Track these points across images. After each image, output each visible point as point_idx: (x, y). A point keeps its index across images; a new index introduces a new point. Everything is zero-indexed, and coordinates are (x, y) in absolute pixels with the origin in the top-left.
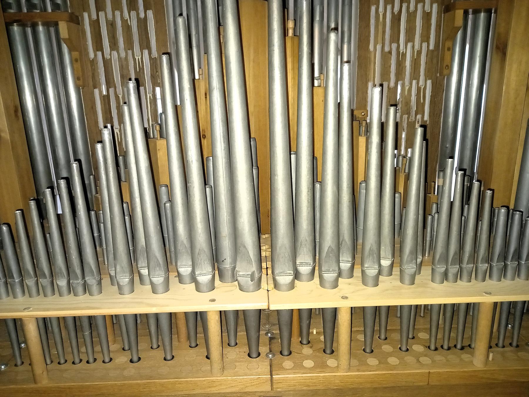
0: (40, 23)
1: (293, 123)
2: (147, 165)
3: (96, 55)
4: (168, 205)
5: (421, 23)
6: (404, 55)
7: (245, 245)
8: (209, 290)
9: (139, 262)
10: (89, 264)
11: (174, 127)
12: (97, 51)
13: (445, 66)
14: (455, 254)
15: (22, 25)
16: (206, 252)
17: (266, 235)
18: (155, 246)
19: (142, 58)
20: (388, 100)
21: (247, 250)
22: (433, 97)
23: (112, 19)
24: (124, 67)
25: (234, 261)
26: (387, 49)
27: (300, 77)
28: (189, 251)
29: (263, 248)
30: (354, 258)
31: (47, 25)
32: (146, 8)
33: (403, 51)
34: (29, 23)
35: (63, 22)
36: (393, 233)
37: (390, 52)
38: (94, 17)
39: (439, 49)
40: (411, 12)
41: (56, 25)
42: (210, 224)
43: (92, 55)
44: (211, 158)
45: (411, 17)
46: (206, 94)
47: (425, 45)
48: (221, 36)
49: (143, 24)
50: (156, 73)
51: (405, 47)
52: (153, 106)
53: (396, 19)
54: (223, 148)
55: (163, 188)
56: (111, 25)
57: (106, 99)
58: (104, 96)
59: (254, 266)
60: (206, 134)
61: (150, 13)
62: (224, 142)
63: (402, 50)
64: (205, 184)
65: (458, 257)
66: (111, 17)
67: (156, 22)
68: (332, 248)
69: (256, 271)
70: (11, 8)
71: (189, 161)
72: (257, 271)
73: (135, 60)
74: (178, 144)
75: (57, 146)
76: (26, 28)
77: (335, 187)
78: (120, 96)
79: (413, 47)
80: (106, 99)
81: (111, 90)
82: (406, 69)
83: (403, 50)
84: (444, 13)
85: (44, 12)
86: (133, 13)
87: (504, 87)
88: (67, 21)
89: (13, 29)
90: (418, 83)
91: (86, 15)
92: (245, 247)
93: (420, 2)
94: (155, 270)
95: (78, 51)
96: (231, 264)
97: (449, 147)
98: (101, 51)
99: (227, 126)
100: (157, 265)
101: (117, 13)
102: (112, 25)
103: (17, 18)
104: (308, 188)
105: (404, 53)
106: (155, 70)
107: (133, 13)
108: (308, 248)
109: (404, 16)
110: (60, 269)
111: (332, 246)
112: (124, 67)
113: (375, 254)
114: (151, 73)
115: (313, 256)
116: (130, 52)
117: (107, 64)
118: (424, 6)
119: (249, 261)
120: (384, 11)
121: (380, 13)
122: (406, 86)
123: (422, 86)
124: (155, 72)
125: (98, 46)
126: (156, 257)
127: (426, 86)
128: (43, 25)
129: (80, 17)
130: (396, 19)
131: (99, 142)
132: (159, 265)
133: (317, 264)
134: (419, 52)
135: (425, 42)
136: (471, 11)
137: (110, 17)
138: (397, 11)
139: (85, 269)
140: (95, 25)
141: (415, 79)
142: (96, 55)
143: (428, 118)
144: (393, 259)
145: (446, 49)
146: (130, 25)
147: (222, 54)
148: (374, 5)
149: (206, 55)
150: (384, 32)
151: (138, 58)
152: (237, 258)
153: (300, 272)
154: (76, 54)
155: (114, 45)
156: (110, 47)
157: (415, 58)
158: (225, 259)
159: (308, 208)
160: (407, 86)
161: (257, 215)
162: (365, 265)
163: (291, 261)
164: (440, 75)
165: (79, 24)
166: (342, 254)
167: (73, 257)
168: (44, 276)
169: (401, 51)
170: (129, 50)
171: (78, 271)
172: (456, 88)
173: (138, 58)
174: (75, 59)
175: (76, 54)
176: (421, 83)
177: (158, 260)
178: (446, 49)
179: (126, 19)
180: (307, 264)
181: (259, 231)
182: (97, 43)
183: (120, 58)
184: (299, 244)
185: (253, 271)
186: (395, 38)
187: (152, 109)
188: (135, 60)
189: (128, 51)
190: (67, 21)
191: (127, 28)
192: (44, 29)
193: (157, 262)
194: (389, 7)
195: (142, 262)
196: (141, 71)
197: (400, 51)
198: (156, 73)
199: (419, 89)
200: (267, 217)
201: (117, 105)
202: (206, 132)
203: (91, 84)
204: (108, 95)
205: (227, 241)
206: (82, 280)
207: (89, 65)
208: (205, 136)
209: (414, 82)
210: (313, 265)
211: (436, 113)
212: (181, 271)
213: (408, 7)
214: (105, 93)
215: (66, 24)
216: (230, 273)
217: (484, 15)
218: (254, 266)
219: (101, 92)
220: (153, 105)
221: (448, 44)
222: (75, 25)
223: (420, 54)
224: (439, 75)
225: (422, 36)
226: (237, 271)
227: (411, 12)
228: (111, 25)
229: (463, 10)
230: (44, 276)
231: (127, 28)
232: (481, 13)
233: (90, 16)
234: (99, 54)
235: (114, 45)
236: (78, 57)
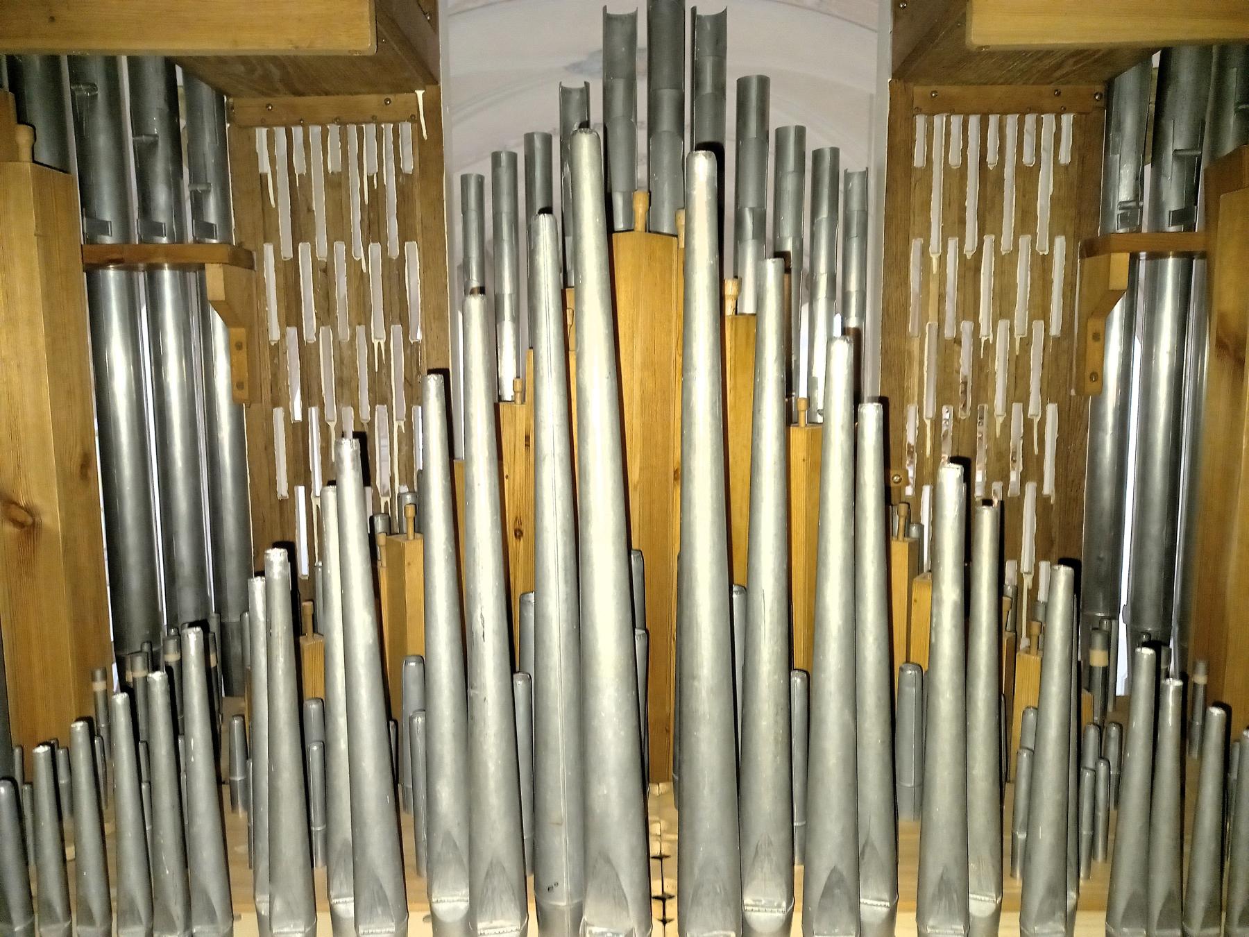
0: (166, 265)
1: (739, 522)
2: (371, 641)
3: (283, 335)
4: (419, 721)
5: (1029, 278)
6: (990, 347)
7: (611, 856)
8: (528, 596)
9: (335, 882)
10: (205, 893)
11: (445, 544)
12: (288, 325)
13: (1088, 374)
14: (1169, 898)
15: (127, 266)
16: (507, 870)
17: (660, 785)
18: (376, 831)
19: (387, 344)
20: (956, 448)
21: (614, 869)
22: (1061, 442)
23: (327, 258)
24: (344, 365)
25: (581, 890)
26: (949, 333)
27: (758, 435)
28: (465, 860)
29: (655, 829)
30: (895, 891)
31: (181, 268)
32: (404, 237)
33: (988, 340)
34: (141, 266)
35: (214, 265)
36: (998, 826)
37: (957, 341)
38: (287, 253)
39: (1073, 336)
40: (1003, 253)
41: (201, 267)
42: (519, 781)
43: (275, 335)
44: (532, 596)
45: (1005, 265)
46: (527, 438)
47: (1039, 325)
48: (569, 312)
49: (394, 271)
50: (416, 376)
51: (991, 329)
52: (405, 448)
53: (970, 269)
54: (562, 596)
55: (413, 664)
56: (324, 272)
57: (299, 433)
58: (295, 424)
59: (631, 913)
60: (523, 528)
61: (412, 250)
62: (566, 582)
63: (986, 336)
64: (513, 671)
65: (1177, 907)
66: (326, 254)
67: (425, 268)
68: (841, 875)
69: (636, 928)
70: (106, 232)
71: (476, 633)
72: (639, 927)
73: (371, 346)
74: (451, 583)
75: (176, 533)
76: (135, 273)
77: (847, 711)
78: (332, 425)
79: (1011, 330)
80: (299, 433)
81: (314, 412)
82: (995, 379)
83: (989, 336)
84: (1082, 257)
85: (177, 243)
86: (375, 248)
87: (1244, 437)
88: (226, 264)
89: (105, 276)
90: (1025, 410)
91: (269, 249)
92: (608, 861)
93: (1023, 233)
94: (371, 912)
95: (244, 326)
96: (571, 896)
97: (1106, 558)
98: (297, 326)
99: (574, 544)
100: (379, 900)
101: (340, 247)
102: (325, 271)
103: (115, 256)
104: (776, 705)
105: (991, 342)
106: (415, 369)
107: (375, 248)
108: (774, 863)
109: (988, 265)
110: (132, 903)
111: (839, 867)
112: (344, 365)
113: (956, 891)
114: (407, 376)
115: (786, 883)
116: (360, 330)
117: (307, 354)
118: (1033, 242)
119: (619, 900)
120: (941, 251)
121: (931, 255)
122: (998, 416)
123: (1035, 418)
124: (415, 374)
125: (292, 316)
126: (377, 880)
127: (1045, 419)
128: (172, 268)
129: (255, 254)
130: (970, 269)
131: (257, 574)
132: (383, 900)
133: (799, 905)
134: (1026, 343)
135: (1039, 319)
136: (1143, 255)
137: (322, 253)
138: (972, 251)
139: (194, 902)
140: (289, 271)
141: (1018, 401)
142: (283, 335)
143: (1052, 491)
144: (999, 899)
145: (1090, 338)
146: (365, 271)
147: (570, 352)
148: (918, 239)
149: (532, 350)
150: (941, 297)
151: (379, 344)
152: (588, 889)
153: (753, 926)
154: (240, 333)
155: (326, 313)
156: (316, 318)
157: (1017, 353)
158: (557, 884)
159: (775, 757)
160: (1000, 416)
161: (641, 750)
162: (929, 919)
163: (729, 905)
164: (1077, 392)
165: (251, 267)
166: (866, 880)
167: (167, 872)
168: (87, 918)
169: (983, 339)
170: (359, 324)
171: (177, 909)
172: (1167, 491)
173: (379, 344)
174: (237, 343)
175: (240, 333)
176: (1033, 408)
177: (381, 886)
178: (1090, 338)
179: (358, 259)
180: (769, 906)
181: (645, 779)
182: (288, 308)
183: (338, 344)
184: (750, 852)
185: (629, 929)
186: (969, 309)
187: (402, 454)
188: (371, 346)
189: (357, 327)
190: (226, 264)
191: (359, 279)
192: (174, 276)
193: (378, 893)
194: (952, 244)
195: (341, 884)
196: (383, 372)
197: (981, 339)
198: (416, 376)
199: (1028, 424)
200: (665, 732)
201: (324, 445)
202: (524, 522)
203: (267, 394)
204: (305, 423)
205: (563, 836)
206: (185, 931)
207: (267, 353)
208: (521, 533)
209: (1017, 408)
210: (787, 907)
211: (1070, 478)
212: (440, 909)
213: (997, 244)
214: (298, 416)
215: (221, 271)
216: (567, 920)
217: (1175, 265)
218: (631, 913)
219: (288, 415)
220: (406, 445)
221: (1093, 325)
222: (243, 269)
223: (1027, 344)
224: (1076, 393)
225: (1031, 306)
226: (586, 924)
227: (1003, 253)
228: (324, 272)
229: (1129, 254)
230: (87, 918)
231: (359, 279)
232: (1169, 257)
233: (277, 252)
234: (292, 331)
235: (326, 313)
236: (244, 340)
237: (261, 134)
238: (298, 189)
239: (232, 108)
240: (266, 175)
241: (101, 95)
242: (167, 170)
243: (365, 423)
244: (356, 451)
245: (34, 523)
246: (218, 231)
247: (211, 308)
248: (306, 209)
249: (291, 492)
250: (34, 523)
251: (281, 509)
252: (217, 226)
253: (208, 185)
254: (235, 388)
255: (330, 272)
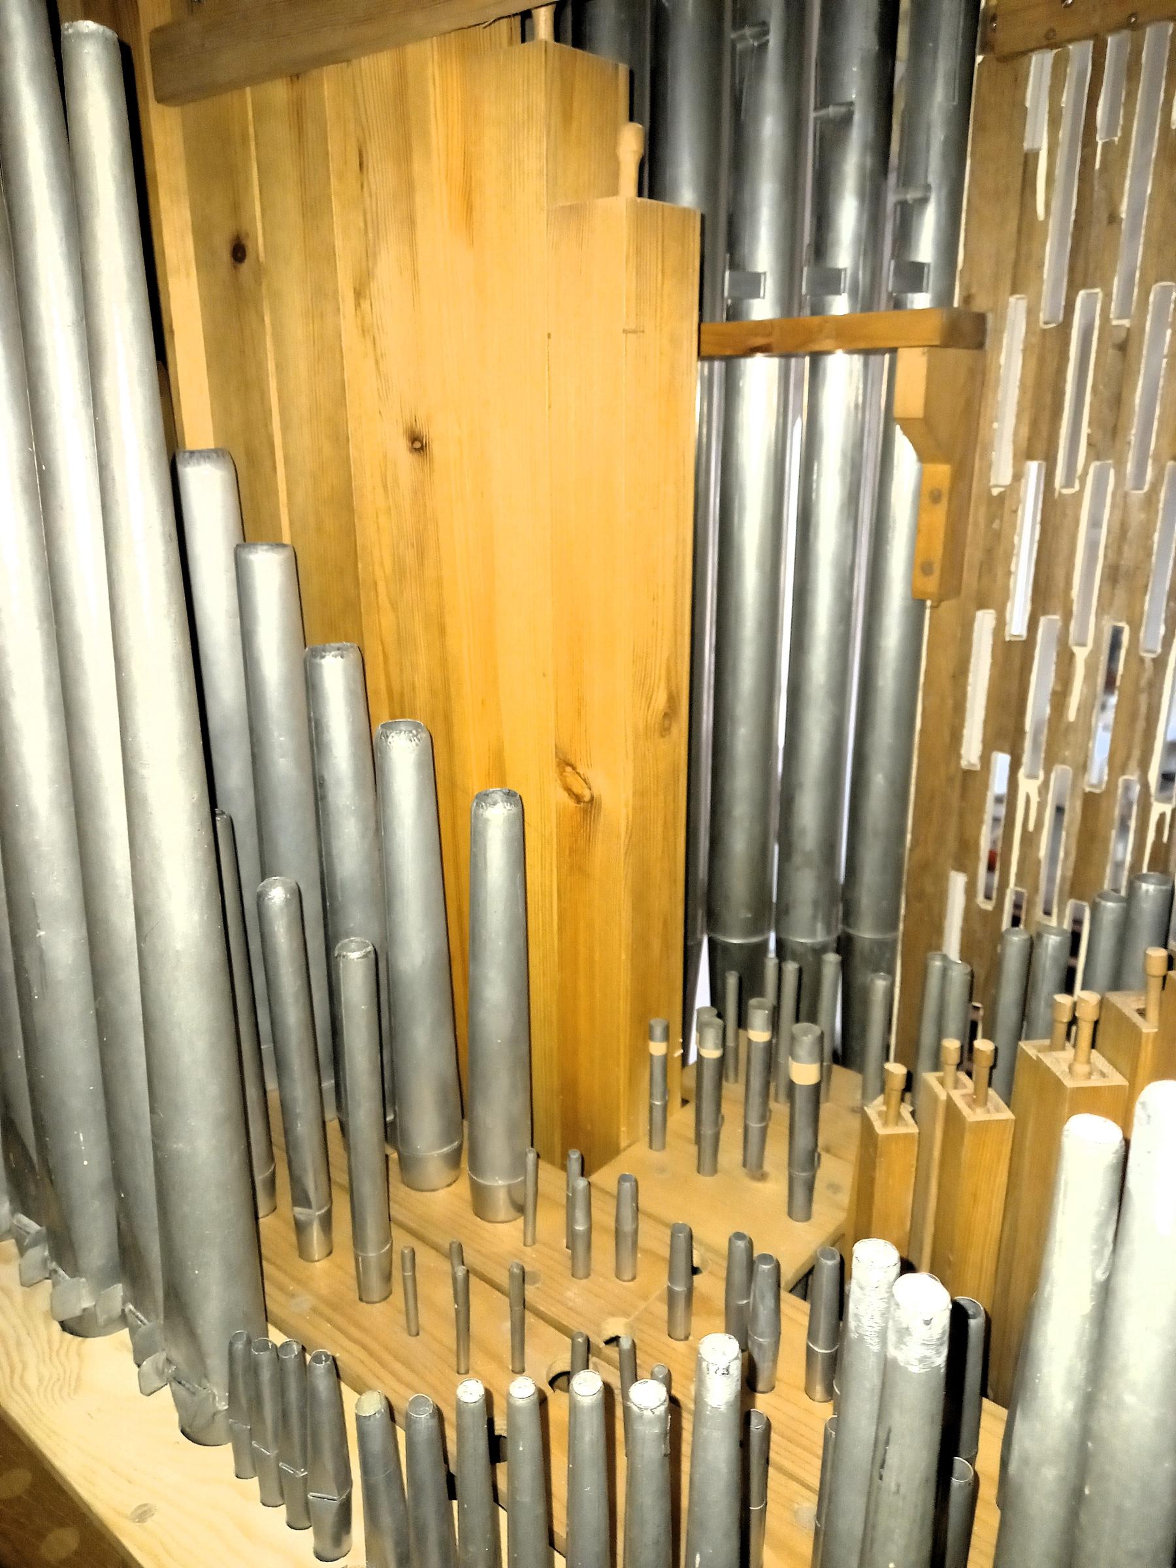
3: (1018, 476)
43: (1002, 474)
142: (1018, 476)
154: (942, 472)
165: (980, 345)
174: (932, 492)
182: (1034, 424)
237: (1040, 64)
238: (1096, 175)
239: (994, 18)
240: (1036, 155)
241: (774, 40)
242: (862, 167)
243: (1148, 656)
244: (955, 107)
245: (592, 798)
246: (932, 278)
247: (898, 428)
248: (1104, 216)
249: (985, 759)
250: (592, 798)
251: (964, 788)
252: (932, 269)
253: (928, 188)
254: (918, 571)
255: (1132, 350)
